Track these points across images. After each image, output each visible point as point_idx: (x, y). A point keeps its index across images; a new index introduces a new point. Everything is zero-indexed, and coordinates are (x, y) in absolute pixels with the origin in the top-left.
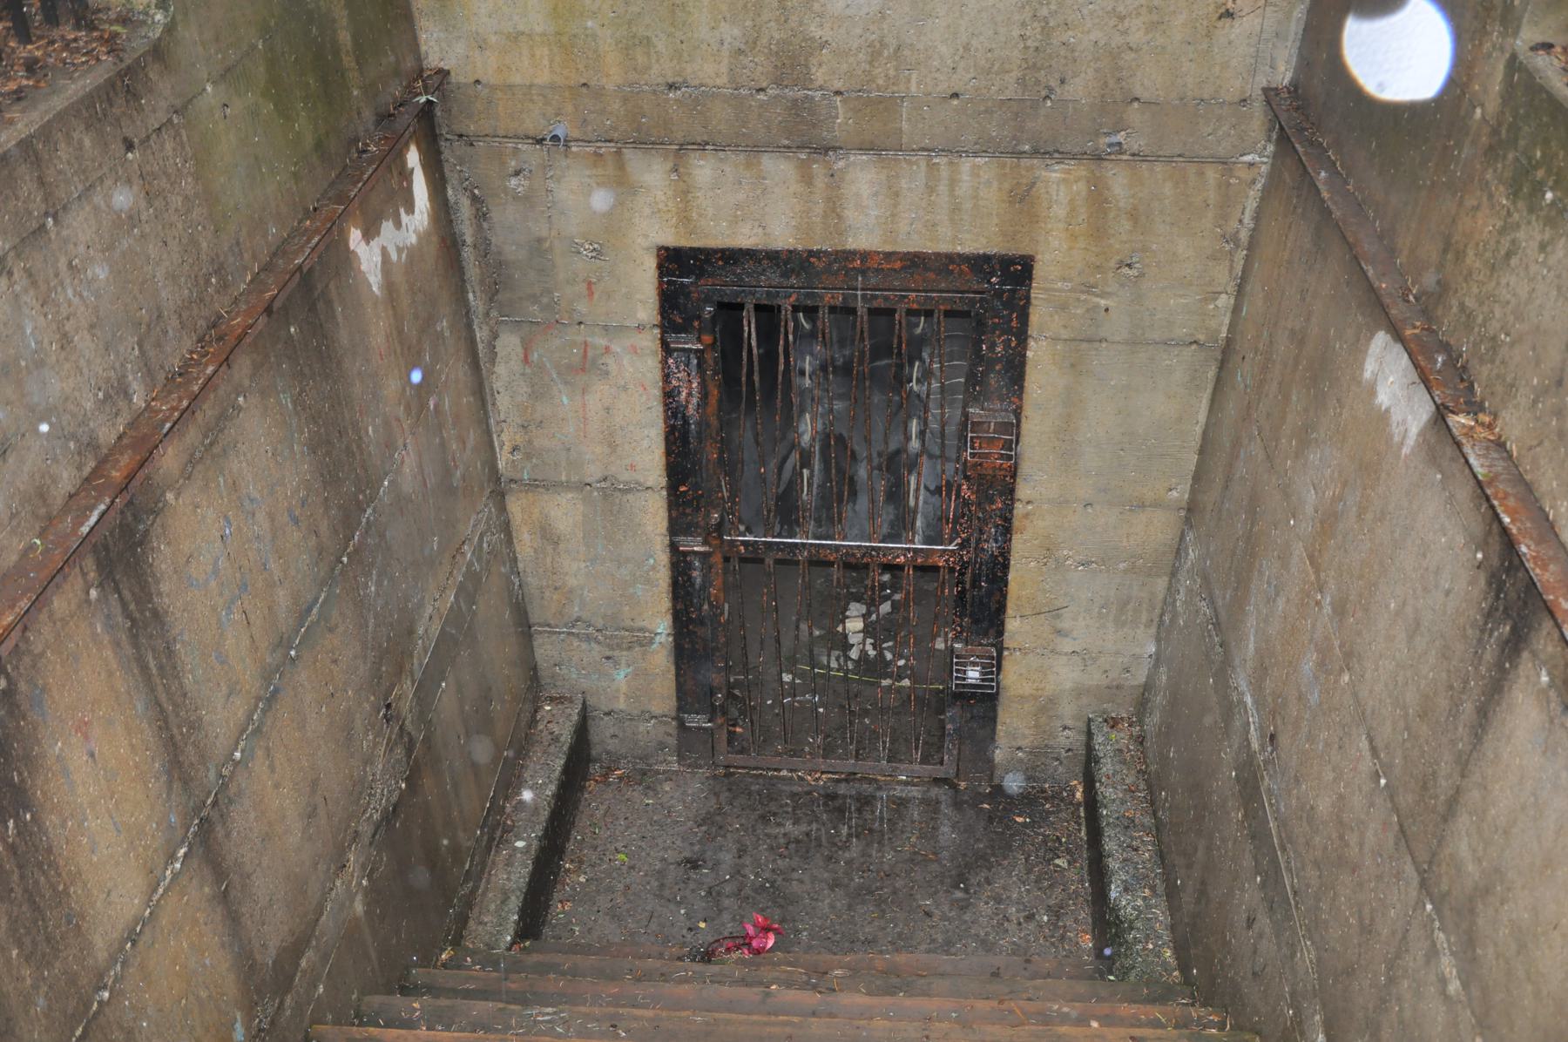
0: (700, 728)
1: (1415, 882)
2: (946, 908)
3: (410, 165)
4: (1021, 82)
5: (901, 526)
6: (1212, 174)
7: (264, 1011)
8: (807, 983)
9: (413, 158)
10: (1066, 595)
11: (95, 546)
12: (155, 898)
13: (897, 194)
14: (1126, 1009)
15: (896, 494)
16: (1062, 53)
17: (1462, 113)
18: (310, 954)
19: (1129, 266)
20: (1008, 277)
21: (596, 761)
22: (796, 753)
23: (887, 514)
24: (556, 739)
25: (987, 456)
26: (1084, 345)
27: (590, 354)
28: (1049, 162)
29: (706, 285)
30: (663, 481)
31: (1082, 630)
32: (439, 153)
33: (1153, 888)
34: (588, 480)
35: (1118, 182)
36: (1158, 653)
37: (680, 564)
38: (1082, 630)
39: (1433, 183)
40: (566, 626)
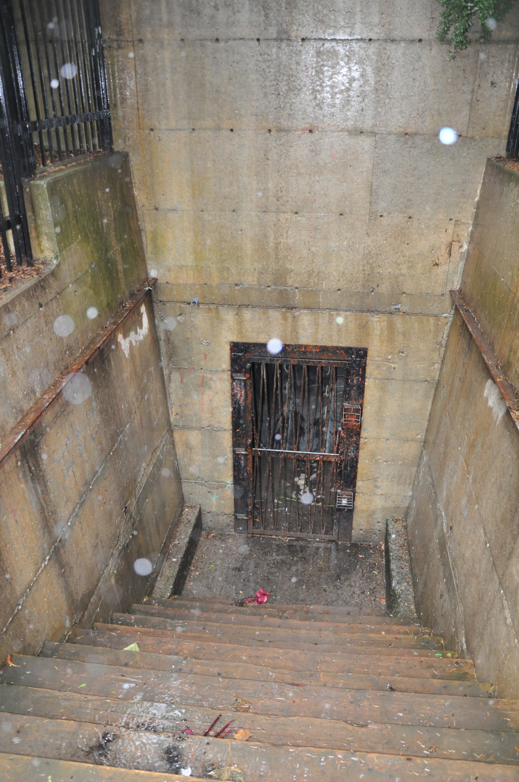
0: (243, 519)
1: (498, 581)
2: (332, 588)
3: (142, 311)
4: (363, 286)
5: (322, 445)
6: (432, 320)
7: (77, 616)
8: (278, 615)
9: (143, 309)
10: (379, 473)
11: (20, 446)
12: (38, 574)
13: (318, 325)
14: (395, 628)
15: (319, 434)
16: (378, 276)
17: (515, 303)
18: (94, 597)
19: (402, 352)
20: (358, 355)
21: (204, 530)
22: (277, 529)
23: (316, 441)
24: (189, 522)
25: (350, 421)
26: (386, 381)
27: (205, 380)
28: (373, 314)
29: (248, 356)
30: (231, 427)
31: (385, 486)
32: (153, 307)
33: (408, 583)
34: (203, 426)
35: (398, 321)
36: (412, 495)
37: (236, 458)
38: (385, 486)
39: (506, 327)
40: (194, 480)
